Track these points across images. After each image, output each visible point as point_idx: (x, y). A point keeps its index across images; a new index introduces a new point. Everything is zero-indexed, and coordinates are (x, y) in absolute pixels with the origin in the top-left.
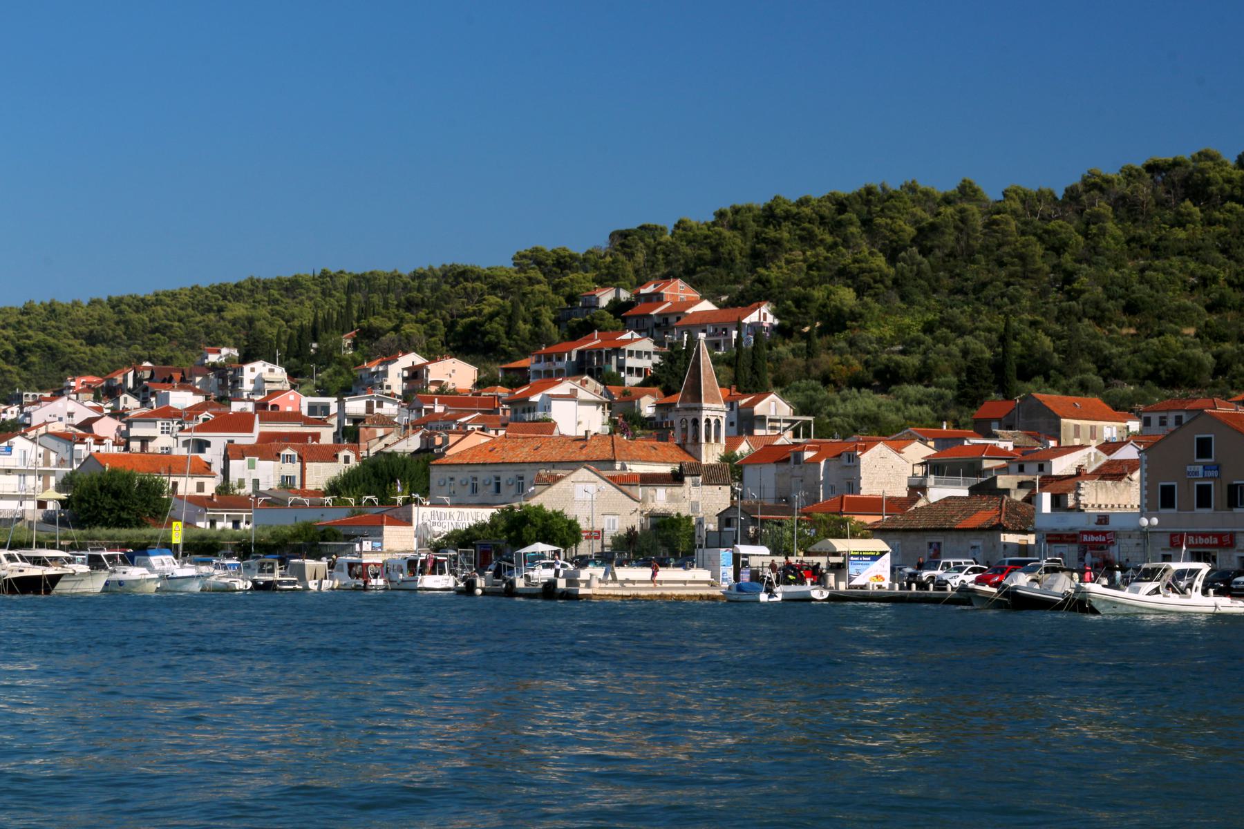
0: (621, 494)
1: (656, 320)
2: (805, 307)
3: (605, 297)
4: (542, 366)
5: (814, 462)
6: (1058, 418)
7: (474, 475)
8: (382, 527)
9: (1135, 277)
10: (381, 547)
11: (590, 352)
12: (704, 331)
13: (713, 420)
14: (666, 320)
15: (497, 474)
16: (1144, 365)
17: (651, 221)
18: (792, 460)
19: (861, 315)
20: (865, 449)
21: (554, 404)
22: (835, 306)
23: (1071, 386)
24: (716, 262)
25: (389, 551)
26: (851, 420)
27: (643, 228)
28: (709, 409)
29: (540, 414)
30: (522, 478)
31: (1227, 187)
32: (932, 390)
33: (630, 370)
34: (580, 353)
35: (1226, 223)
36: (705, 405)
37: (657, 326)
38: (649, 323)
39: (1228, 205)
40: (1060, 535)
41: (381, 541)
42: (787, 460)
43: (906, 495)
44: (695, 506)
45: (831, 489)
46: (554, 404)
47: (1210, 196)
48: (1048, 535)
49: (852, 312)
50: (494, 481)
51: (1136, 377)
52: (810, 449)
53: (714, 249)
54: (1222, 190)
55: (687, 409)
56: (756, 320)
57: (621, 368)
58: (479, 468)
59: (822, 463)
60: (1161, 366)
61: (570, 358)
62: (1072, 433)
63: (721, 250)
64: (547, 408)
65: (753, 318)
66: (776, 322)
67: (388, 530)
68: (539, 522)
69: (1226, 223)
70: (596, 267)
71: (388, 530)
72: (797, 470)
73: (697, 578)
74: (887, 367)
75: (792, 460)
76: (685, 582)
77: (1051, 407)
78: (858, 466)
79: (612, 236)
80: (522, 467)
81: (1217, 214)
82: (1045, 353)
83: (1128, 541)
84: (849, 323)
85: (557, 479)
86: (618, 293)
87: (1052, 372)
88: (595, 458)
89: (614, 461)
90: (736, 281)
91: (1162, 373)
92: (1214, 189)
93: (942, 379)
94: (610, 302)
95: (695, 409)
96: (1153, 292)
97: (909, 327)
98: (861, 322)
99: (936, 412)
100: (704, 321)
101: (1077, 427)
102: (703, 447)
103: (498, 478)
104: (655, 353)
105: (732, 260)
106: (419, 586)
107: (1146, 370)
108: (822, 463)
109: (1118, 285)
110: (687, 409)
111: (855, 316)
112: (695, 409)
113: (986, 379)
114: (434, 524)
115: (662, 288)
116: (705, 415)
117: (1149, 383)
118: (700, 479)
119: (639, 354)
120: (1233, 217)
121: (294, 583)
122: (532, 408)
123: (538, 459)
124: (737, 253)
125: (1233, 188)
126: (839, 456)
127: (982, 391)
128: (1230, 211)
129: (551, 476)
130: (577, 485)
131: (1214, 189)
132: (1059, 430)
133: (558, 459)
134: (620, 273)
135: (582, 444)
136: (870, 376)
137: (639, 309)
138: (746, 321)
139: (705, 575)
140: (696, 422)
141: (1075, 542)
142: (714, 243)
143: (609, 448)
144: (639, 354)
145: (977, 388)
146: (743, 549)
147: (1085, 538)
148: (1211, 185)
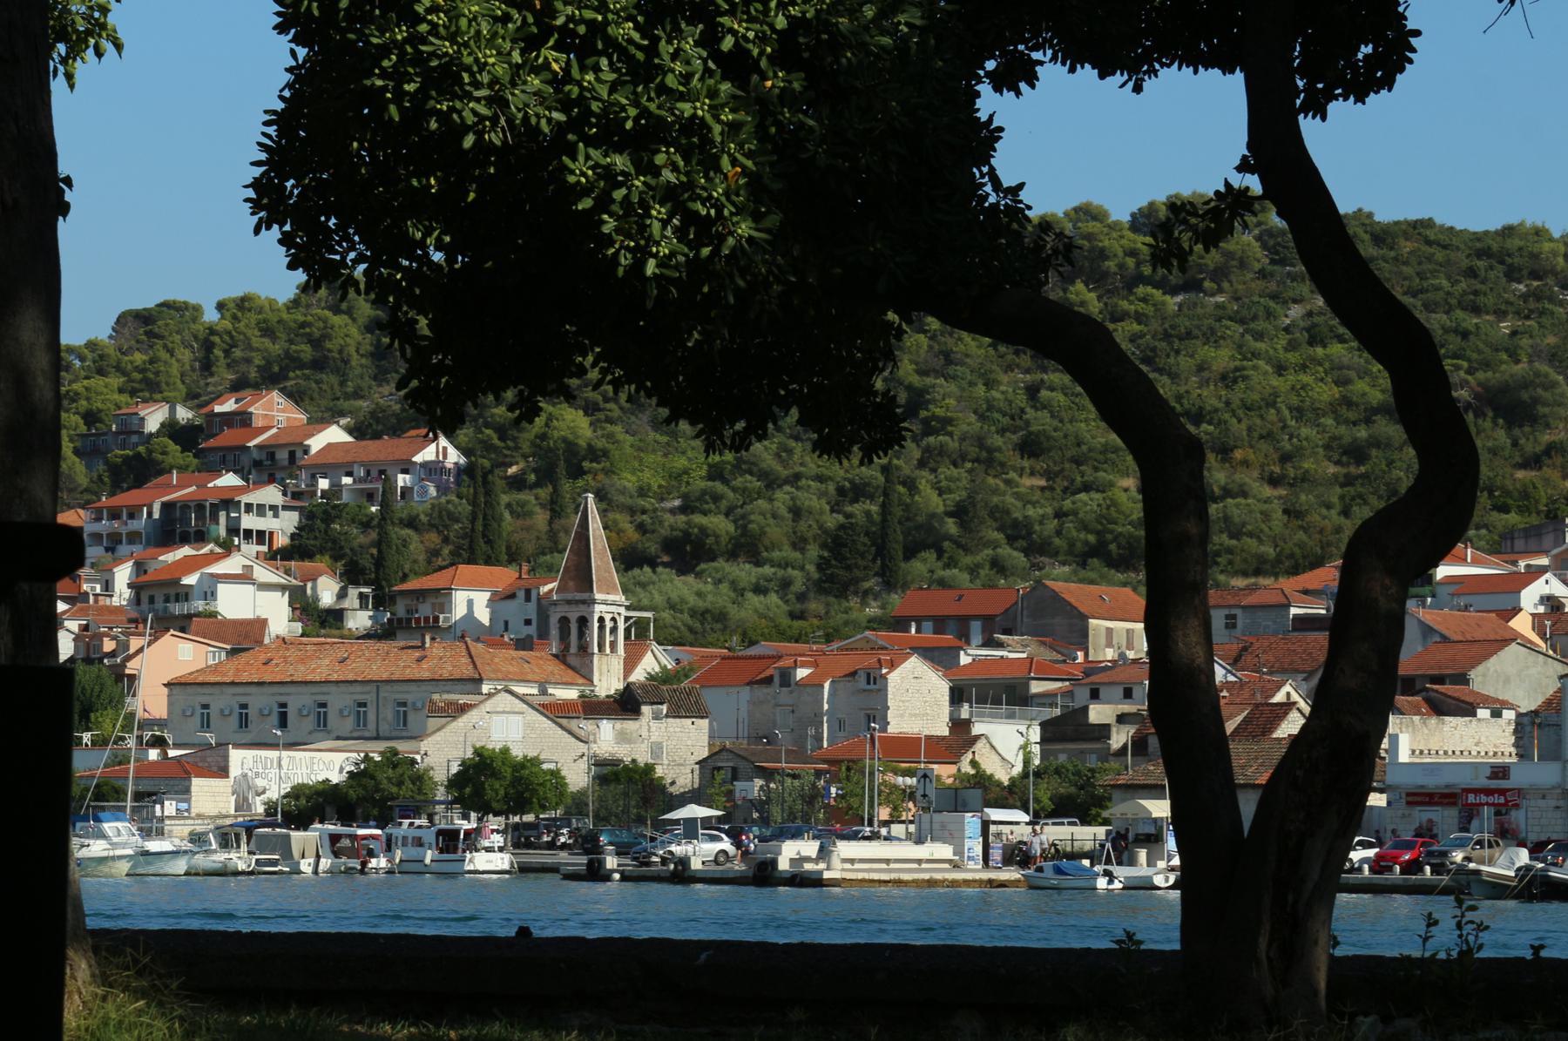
0: (560, 731)
1: (255, 455)
2: (514, 439)
3: (154, 419)
4: (105, 526)
5: (814, 685)
6: (1084, 618)
7: (243, 700)
8: (189, 779)
9: (1021, 400)
10: (188, 810)
11: (185, 506)
12: (349, 474)
13: (608, 617)
14: (272, 456)
15: (283, 699)
16: (1082, 535)
17: (179, 296)
18: (777, 680)
19: (605, 453)
20: (893, 666)
21: (222, 588)
22: (565, 440)
23: (978, 566)
24: (319, 364)
25: (199, 816)
26: (686, 617)
27: (165, 305)
28: (605, 603)
29: (199, 605)
30: (324, 705)
31: (1130, 262)
32: (767, 570)
33: (248, 534)
34: (166, 506)
35: (1139, 318)
36: (598, 596)
37: (257, 464)
38: (245, 461)
39: (1141, 290)
40: (1431, 795)
41: (188, 801)
42: (768, 681)
43: (946, 733)
44: (656, 749)
45: (839, 725)
46: (222, 588)
47: (1106, 275)
48: (1408, 794)
49: (590, 447)
50: (276, 709)
51: (1070, 552)
52: (804, 665)
53: (316, 343)
54: (1121, 266)
55: (569, 602)
56: (433, 458)
57: (233, 530)
58: (253, 689)
59: (827, 685)
60: (1109, 537)
61: (150, 514)
62: (1103, 641)
63: (328, 345)
64: (210, 595)
65: (428, 454)
66: (463, 460)
67: (197, 784)
68: (507, 772)
69: (1139, 318)
70: (119, 369)
71: (197, 784)
72: (784, 695)
73: (936, 856)
74: (687, 534)
75: (777, 680)
76: (919, 861)
77: (1072, 601)
78: (883, 691)
79: (122, 320)
80: (325, 689)
81: (1124, 304)
82: (933, 515)
83: (1541, 803)
84: (586, 464)
85: (464, 709)
86: (172, 411)
87: (946, 544)
88: (446, 675)
89: (480, 681)
90: (357, 394)
91: (1113, 547)
92: (1111, 265)
93: (776, 554)
94: (163, 425)
95: (584, 602)
96: (1056, 423)
97: (686, 472)
98: (605, 464)
99: (787, 602)
100: (349, 459)
101: (1109, 631)
102: (596, 659)
103: (283, 705)
104: (285, 508)
105: (346, 362)
106: (467, 868)
107: (1086, 543)
108: (827, 685)
109: (1000, 411)
110: (569, 602)
111: (594, 454)
112: (584, 602)
113: (863, 556)
114: (257, 774)
115: (251, 404)
116: (598, 609)
117: (1094, 562)
118: (664, 708)
119: (261, 510)
120: (1149, 310)
121: (274, 863)
122: (185, 595)
123: (351, 677)
124: (352, 350)
125: (1138, 264)
126: (853, 674)
127: (857, 573)
128: (1144, 300)
129: (450, 704)
130: (495, 717)
131: (1111, 265)
132: (1086, 635)
133: (385, 676)
134: (162, 378)
135: (417, 654)
136: (653, 548)
137: (227, 437)
138: (418, 458)
139: (945, 851)
140: (584, 622)
141: (1454, 804)
142: (317, 334)
143: (466, 660)
144: (261, 510)
145: (848, 568)
146: (995, 814)
147: (1471, 798)
148: (1107, 258)
